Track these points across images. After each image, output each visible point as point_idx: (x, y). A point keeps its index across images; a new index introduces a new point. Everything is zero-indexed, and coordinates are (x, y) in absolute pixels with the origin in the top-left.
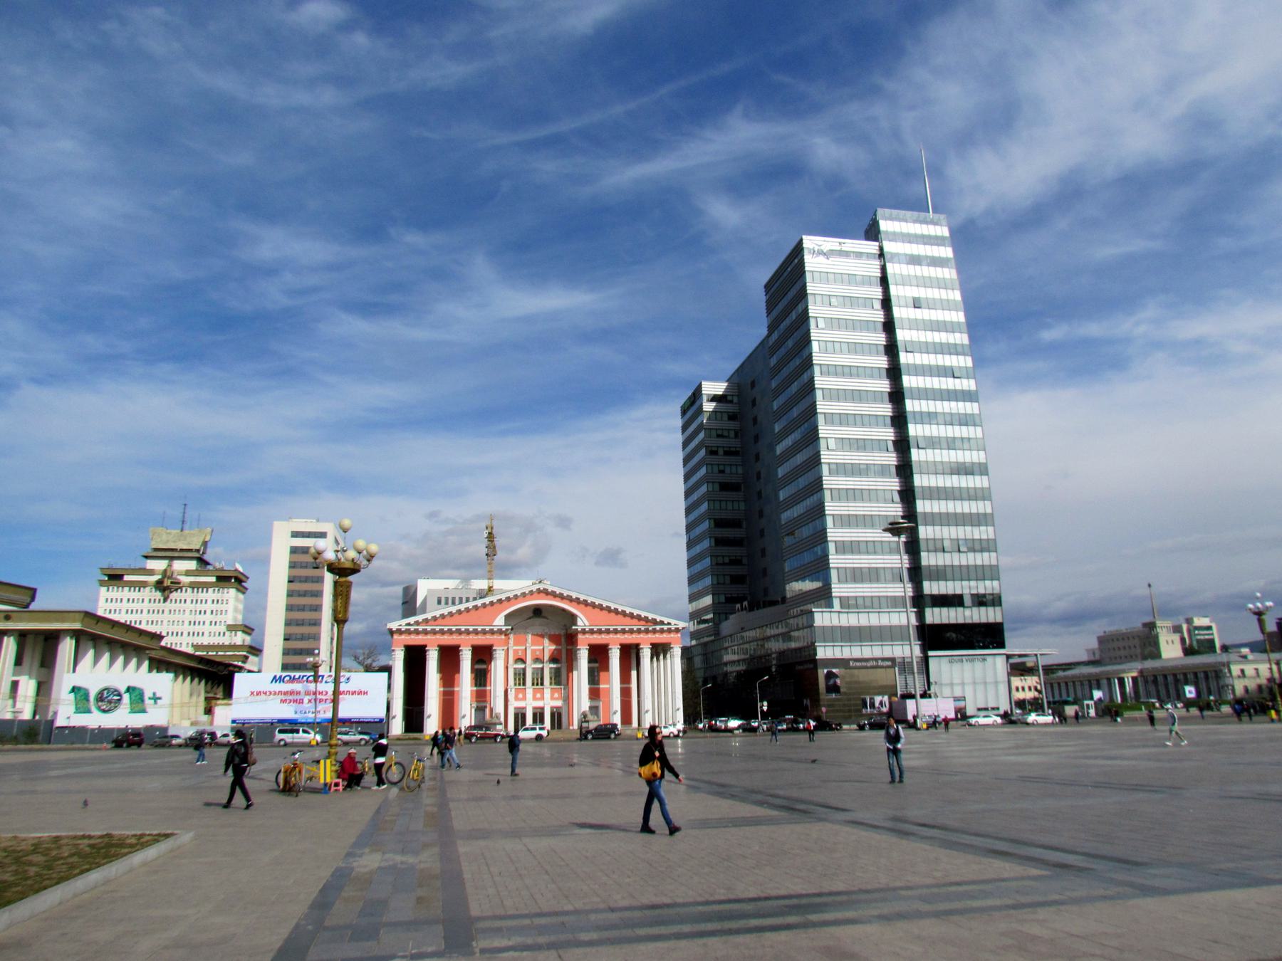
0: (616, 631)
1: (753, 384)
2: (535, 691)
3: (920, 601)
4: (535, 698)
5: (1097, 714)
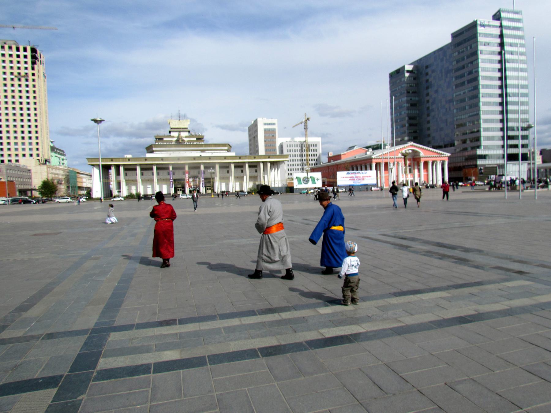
0: (431, 157)
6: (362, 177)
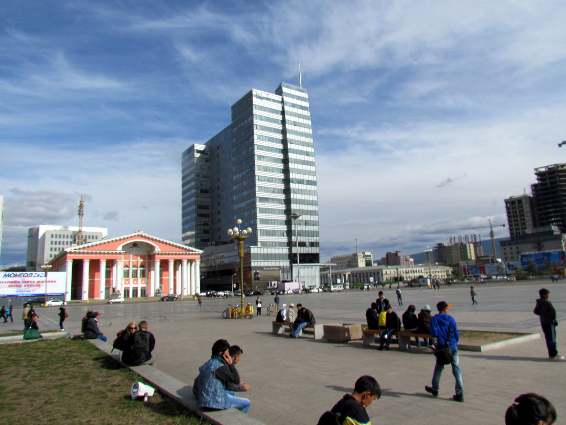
0: (172, 254)
1: (218, 148)
2: (134, 280)
3: (290, 244)
4: (134, 283)
5: (350, 287)
6: (36, 282)
